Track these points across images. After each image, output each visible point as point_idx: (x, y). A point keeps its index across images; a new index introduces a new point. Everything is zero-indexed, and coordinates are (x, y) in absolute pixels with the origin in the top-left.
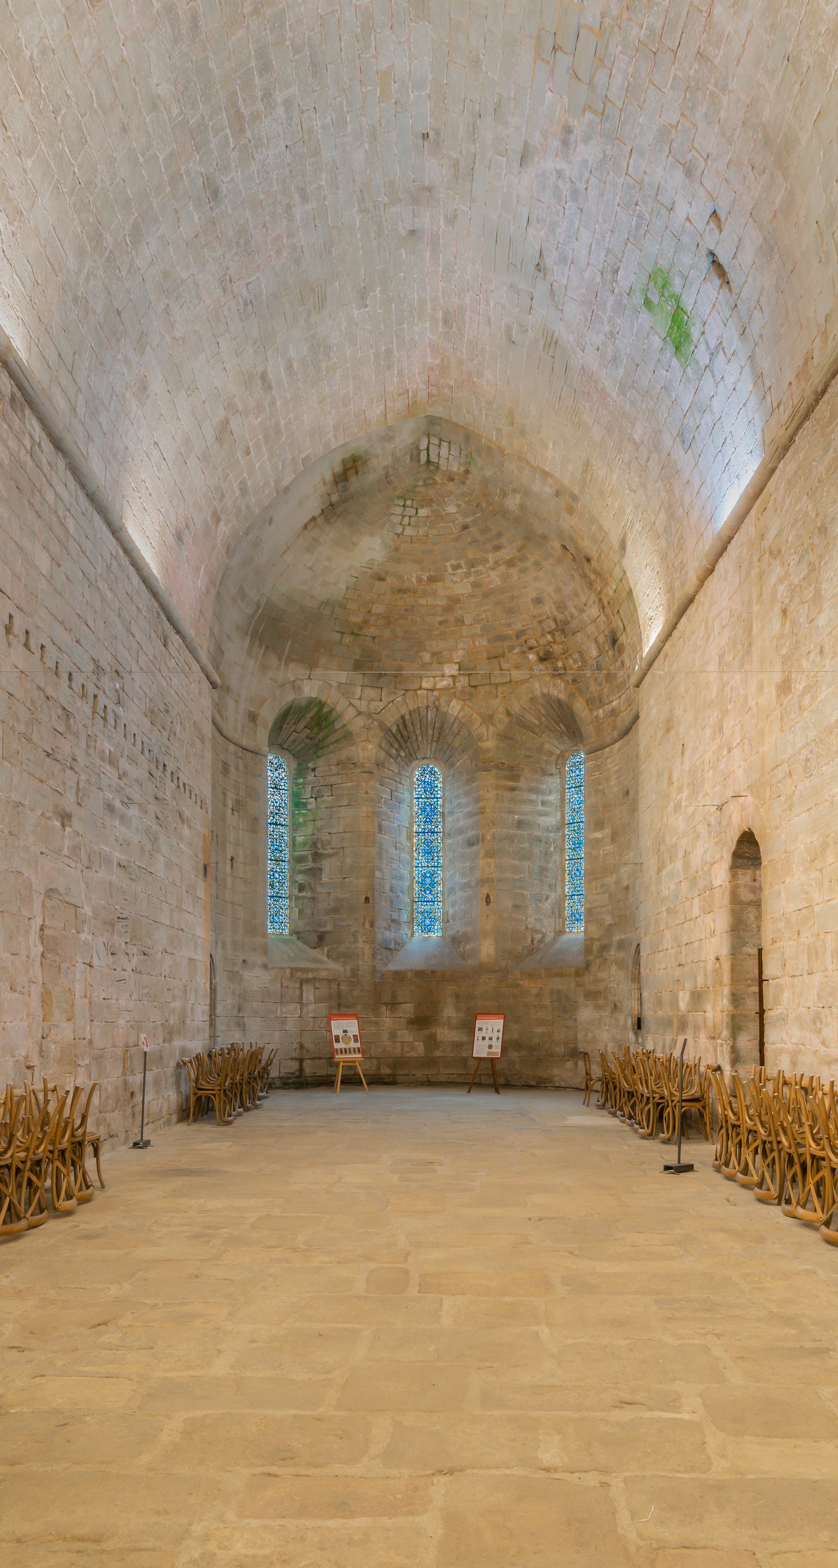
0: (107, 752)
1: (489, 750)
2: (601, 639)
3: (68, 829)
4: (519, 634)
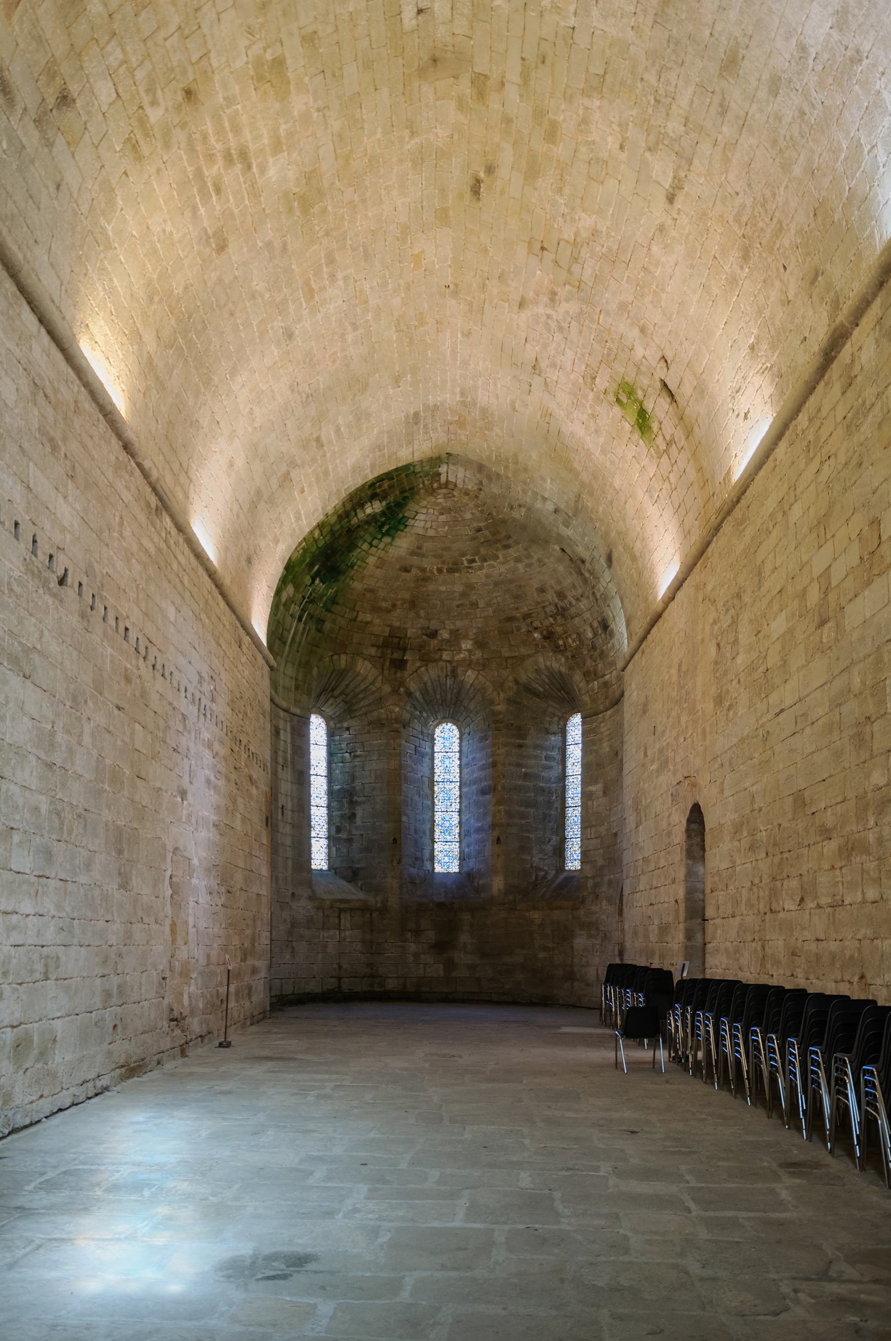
1: (500, 713)
2: (595, 624)
3: (185, 802)
4: (526, 616)
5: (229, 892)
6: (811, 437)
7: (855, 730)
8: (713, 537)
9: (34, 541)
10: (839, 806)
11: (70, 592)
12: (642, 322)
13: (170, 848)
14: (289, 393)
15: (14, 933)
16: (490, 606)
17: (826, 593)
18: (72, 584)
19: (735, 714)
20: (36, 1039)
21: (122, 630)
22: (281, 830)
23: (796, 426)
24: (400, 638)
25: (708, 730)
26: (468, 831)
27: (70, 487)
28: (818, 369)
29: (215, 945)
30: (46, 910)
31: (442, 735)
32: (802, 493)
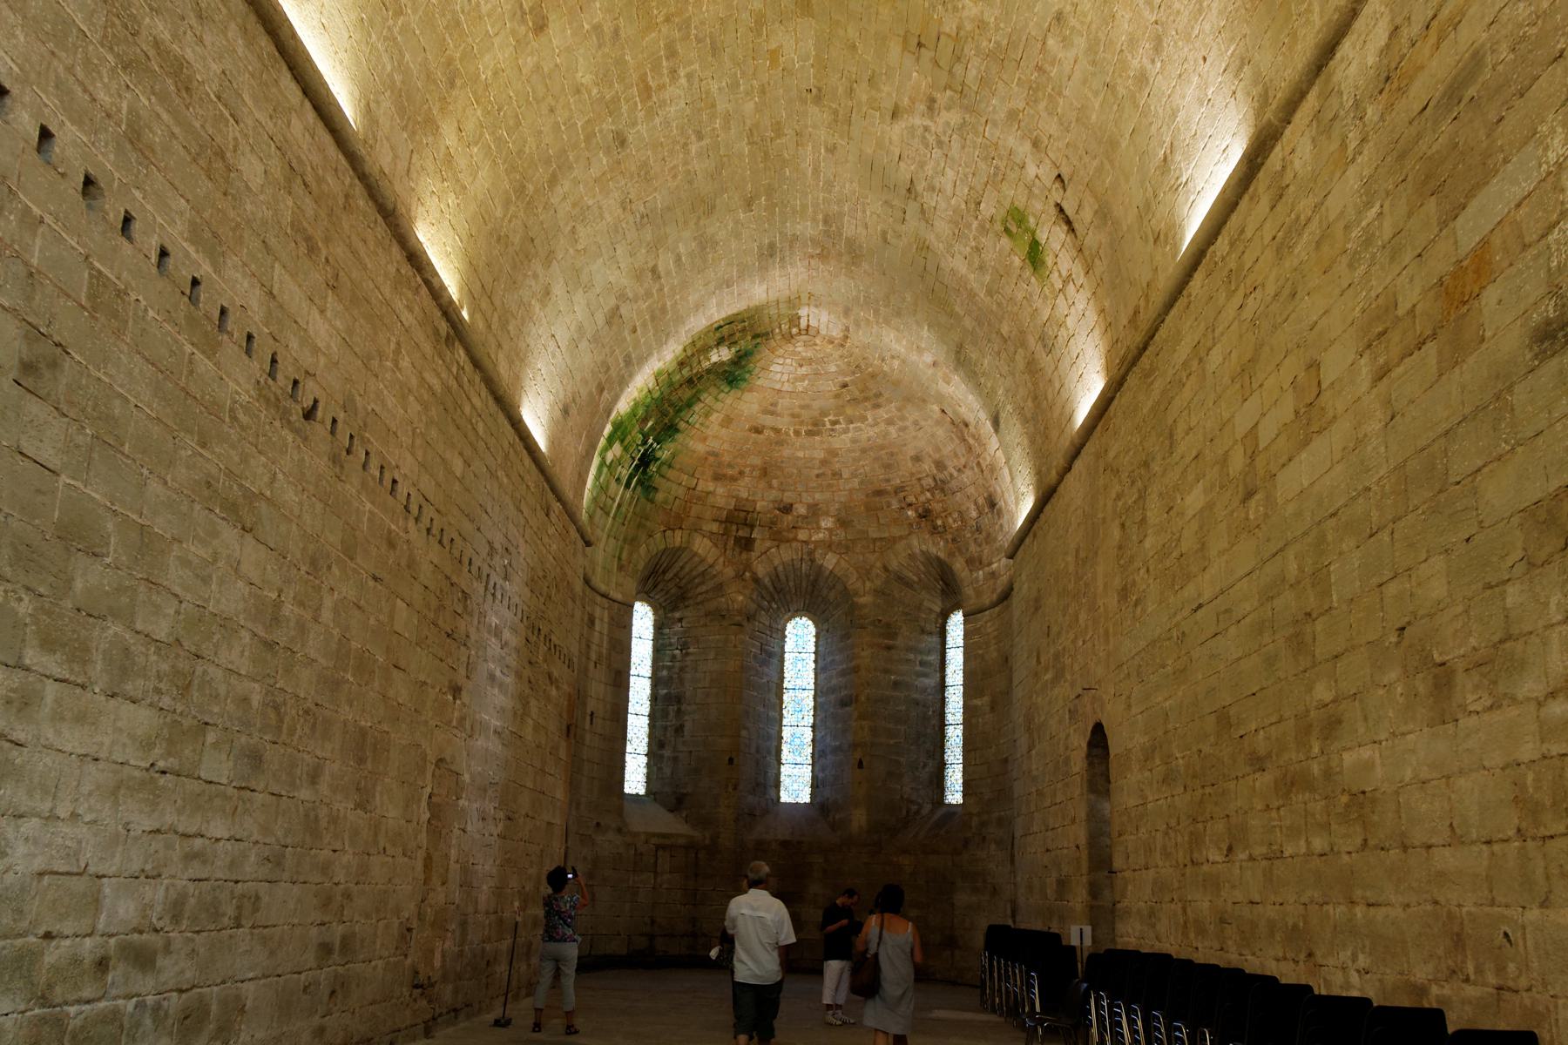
0: (494, 625)
1: (865, 606)
2: (981, 501)
3: (458, 702)
4: (898, 490)
5: (509, 819)
6: (1233, 265)
7: (1291, 630)
8: (1116, 393)
9: (274, 361)
10: (1273, 728)
11: (319, 430)
12: (1035, 134)
13: (432, 758)
14: (620, 211)
15: (196, 864)
16: (856, 477)
17: (1252, 458)
18: (323, 418)
19: (1144, 611)
20: (214, 1008)
21: (387, 483)
22: (587, 742)
23: (1214, 252)
24: (748, 512)
25: (1111, 630)
26: (823, 751)
27: (330, 299)
28: (1241, 180)
29: (485, 887)
30: (245, 834)
31: (795, 631)
32: (1222, 334)
